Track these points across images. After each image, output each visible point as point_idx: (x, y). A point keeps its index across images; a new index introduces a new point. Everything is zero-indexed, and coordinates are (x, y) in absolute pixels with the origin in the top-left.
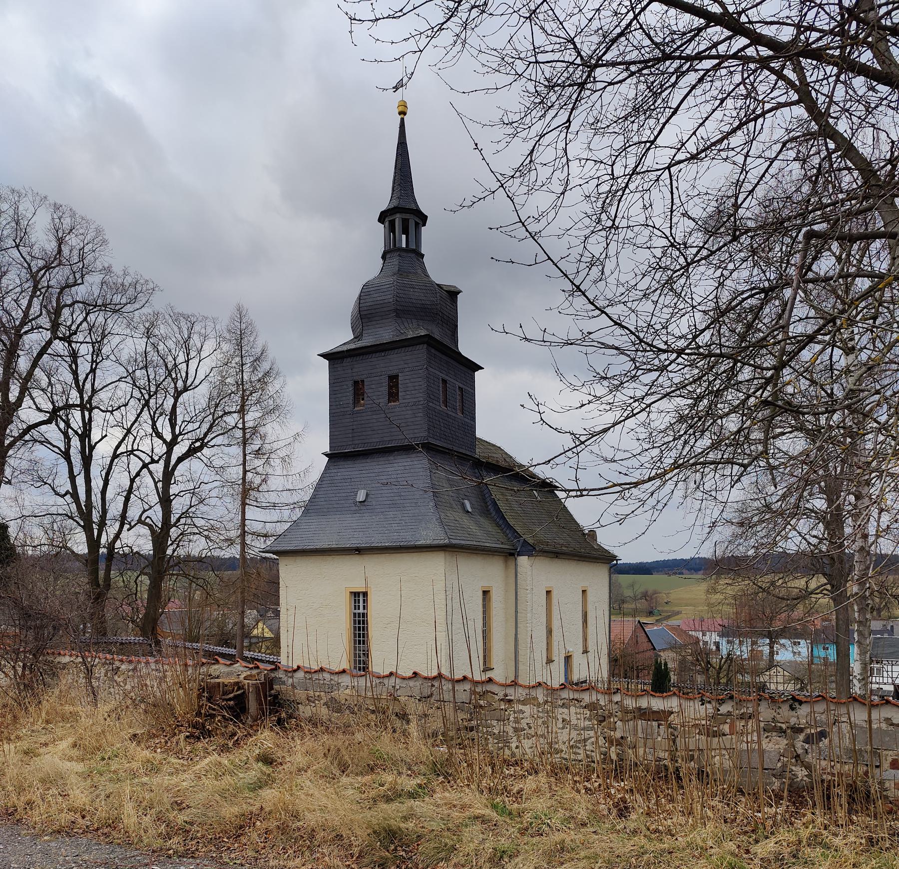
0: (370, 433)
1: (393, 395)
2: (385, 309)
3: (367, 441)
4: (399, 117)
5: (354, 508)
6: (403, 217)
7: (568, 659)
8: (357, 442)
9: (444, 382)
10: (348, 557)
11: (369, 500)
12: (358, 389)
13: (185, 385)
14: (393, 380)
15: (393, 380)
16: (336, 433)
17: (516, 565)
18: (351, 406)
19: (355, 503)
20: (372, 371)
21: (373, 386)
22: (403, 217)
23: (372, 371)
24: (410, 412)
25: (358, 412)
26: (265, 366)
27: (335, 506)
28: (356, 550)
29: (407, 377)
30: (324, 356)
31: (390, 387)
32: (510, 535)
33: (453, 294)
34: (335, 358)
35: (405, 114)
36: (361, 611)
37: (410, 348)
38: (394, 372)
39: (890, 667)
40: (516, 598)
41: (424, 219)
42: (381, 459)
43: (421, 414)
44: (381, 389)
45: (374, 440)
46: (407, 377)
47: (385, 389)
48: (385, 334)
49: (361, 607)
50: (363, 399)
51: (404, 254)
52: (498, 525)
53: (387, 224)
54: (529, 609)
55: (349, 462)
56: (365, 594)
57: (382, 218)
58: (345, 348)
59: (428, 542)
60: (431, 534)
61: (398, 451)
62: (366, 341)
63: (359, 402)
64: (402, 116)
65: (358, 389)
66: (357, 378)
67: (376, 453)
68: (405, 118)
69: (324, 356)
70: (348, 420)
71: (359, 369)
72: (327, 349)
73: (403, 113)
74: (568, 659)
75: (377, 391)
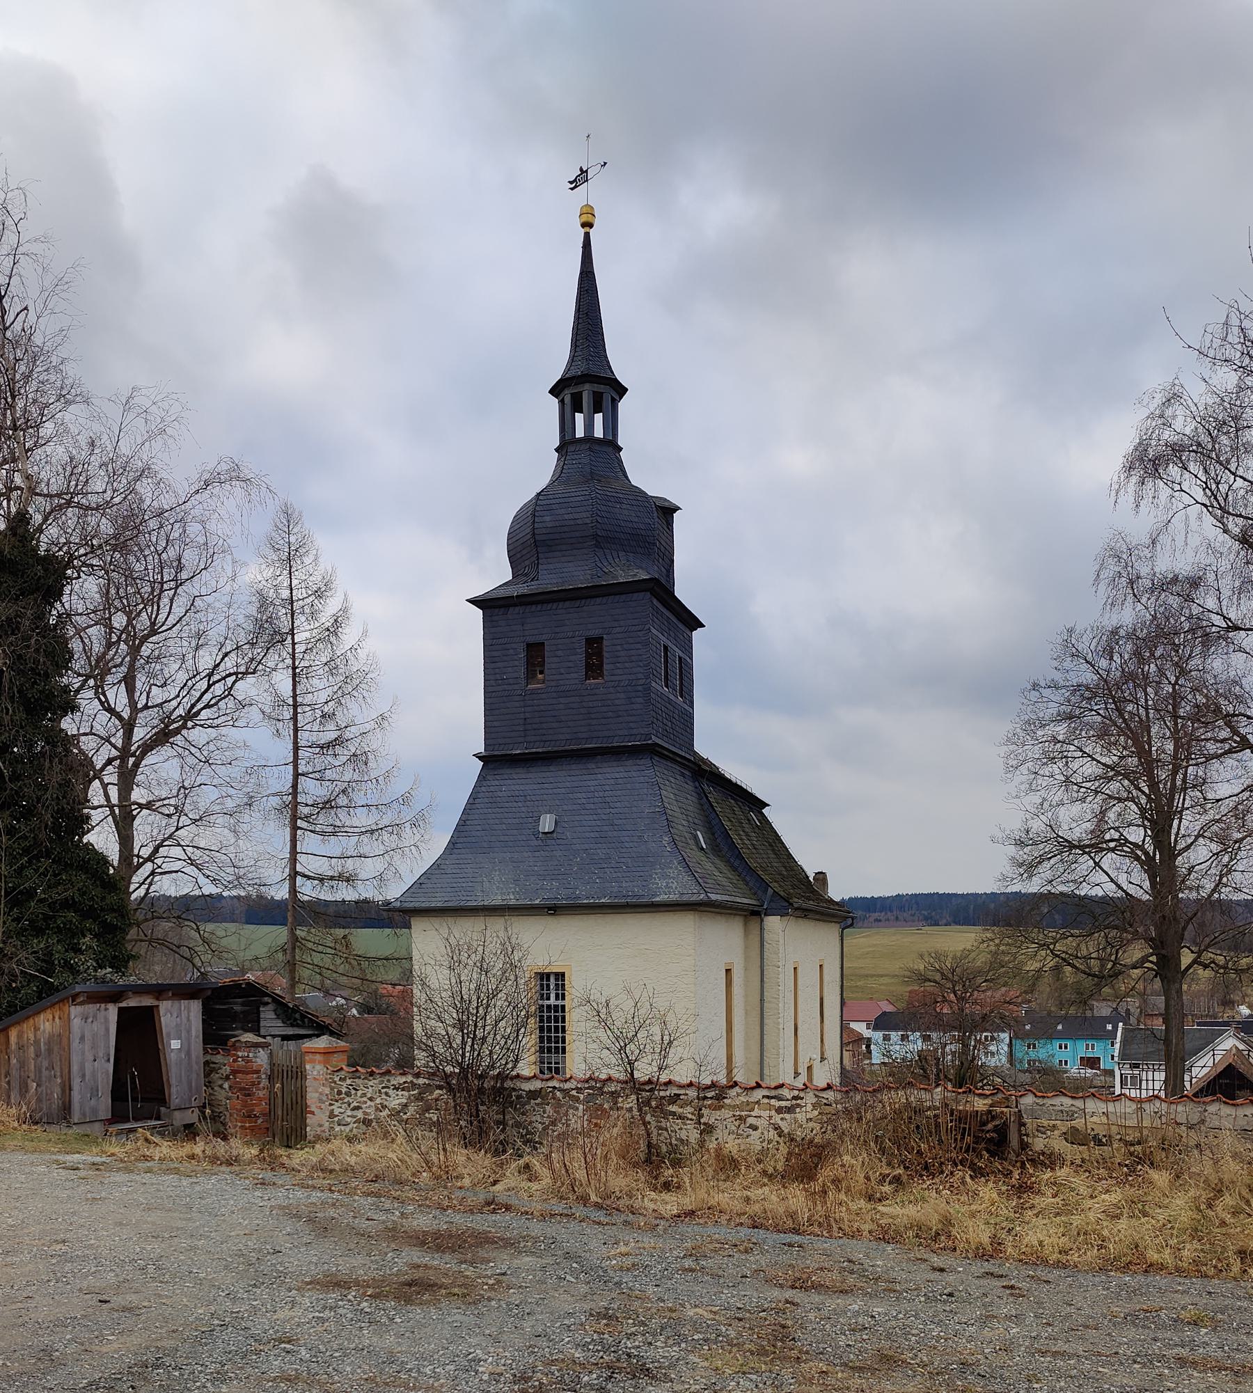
0: (555, 725)
1: (594, 668)
2: (577, 534)
3: (550, 738)
4: (582, 231)
5: (536, 843)
6: (589, 384)
7: (810, 1068)
8: (533, 739)
9: (666, 648)
10: (532, 919)
11: (559, 830)
12: (535, 653)
13: (153, 624)
14: (594, 645)
15: (594, 645)
16: (496, 724)
17: (762, 929)
18: (523, 682)
19: (536, 834)
20: (557, 630)
21: (559, 653)
22: (589, 384)
23: (557, 630)
24: (622, 696)
25: (533, 692)
26: (331, 607)
27: (502, 838)
28: (550, 909)
29: (618, 642)
30: (473, 601)
31: (588, 656)
32: (751, 884)
33: (667, 511)
34: (490, 605)
35: (591, 225)
36: (552, 1001)
37: (623, 597)
38: (594, 633)
39: (1150, 1073)
40: (762, 981)
41: (622, 391)
42: (574, 767)
43: (640, 700)
44: (572, 658)
45: (561, 737)
46: (618, 642)
47: (580, 658)
48: (575, 572)
49: (553, 996)
50: (541, 672)
51: (597, 447)
52: (734, 869)
53: (568, 399)
54: (781, 995)
55: (518, 770)
56: (560, 976)
57: (555, 391)
58: (502, 594)
59: (673, 897)
60: (672, 885)
61: (602, 754)
62: (548, 581)
63: (534, 676)
64: (587, 229)
65: (535, 653)
66: (531, 640)
67: (566, 757)
68: (591, 231)
69: (473, 601)
70: (517, 704)
71: (537, 626)
72: (480, 590)
73: (588, 225)
74: (810, 1068)
75: (565, 663)
